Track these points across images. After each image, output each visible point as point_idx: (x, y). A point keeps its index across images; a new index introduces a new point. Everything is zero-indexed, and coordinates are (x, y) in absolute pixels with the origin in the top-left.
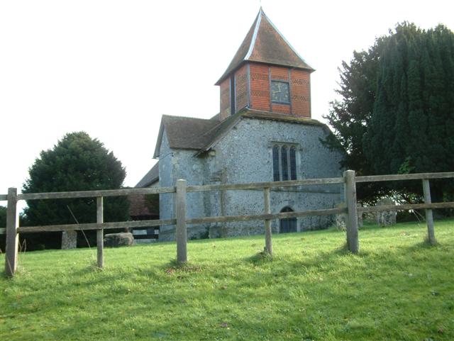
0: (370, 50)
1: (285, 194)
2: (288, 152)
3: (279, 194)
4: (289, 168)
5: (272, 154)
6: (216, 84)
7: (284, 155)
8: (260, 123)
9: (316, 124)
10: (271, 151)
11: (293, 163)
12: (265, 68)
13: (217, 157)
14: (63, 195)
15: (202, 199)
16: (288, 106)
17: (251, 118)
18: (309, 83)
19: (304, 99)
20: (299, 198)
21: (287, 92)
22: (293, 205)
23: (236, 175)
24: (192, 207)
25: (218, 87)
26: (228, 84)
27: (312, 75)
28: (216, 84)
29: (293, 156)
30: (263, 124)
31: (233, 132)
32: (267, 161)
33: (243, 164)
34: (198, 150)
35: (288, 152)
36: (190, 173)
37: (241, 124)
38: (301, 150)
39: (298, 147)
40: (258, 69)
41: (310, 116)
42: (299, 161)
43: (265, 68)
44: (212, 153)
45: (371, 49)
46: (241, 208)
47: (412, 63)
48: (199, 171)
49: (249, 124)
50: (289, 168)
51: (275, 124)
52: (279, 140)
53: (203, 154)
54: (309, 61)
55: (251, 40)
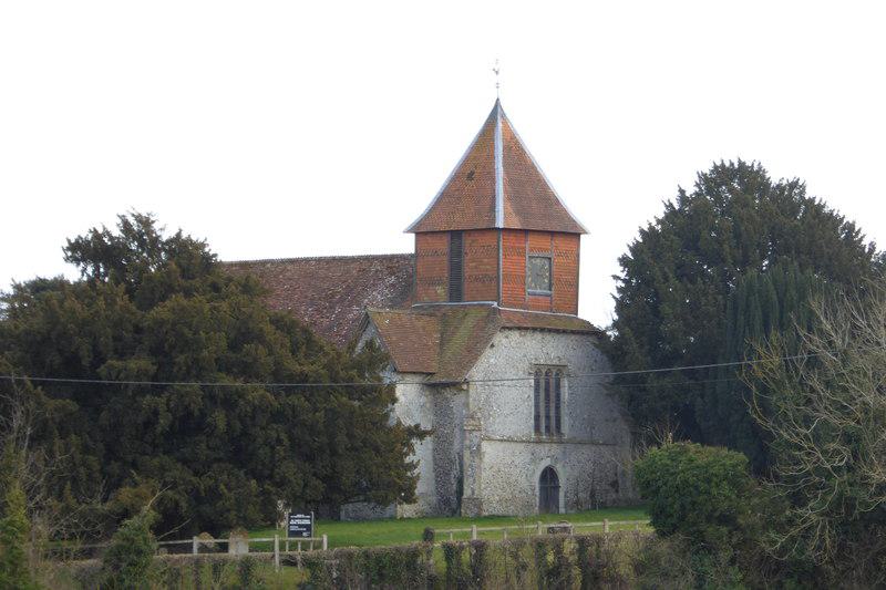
0: (832, 212)
1: (547, 447)
2: (552, 382)
3: (540, 447)
4: (553, 405)
6: (409, 231)
7: (547, 383)
8: (521, 335)
9: (588, 331)
11: (558, 396)
14: (180, 542)
15: (430, 451)
19: (567, 286)
29: (558, 386)
31: (488, 351)
41: (577, 314)
42: (565, 393)
44: (465, 387)
45: (654, 223)
46: (496, 469)
47: (132, 220)
48: (428, 405)
49: (507, 337)
50: (553, 405)
51: (538, 336)
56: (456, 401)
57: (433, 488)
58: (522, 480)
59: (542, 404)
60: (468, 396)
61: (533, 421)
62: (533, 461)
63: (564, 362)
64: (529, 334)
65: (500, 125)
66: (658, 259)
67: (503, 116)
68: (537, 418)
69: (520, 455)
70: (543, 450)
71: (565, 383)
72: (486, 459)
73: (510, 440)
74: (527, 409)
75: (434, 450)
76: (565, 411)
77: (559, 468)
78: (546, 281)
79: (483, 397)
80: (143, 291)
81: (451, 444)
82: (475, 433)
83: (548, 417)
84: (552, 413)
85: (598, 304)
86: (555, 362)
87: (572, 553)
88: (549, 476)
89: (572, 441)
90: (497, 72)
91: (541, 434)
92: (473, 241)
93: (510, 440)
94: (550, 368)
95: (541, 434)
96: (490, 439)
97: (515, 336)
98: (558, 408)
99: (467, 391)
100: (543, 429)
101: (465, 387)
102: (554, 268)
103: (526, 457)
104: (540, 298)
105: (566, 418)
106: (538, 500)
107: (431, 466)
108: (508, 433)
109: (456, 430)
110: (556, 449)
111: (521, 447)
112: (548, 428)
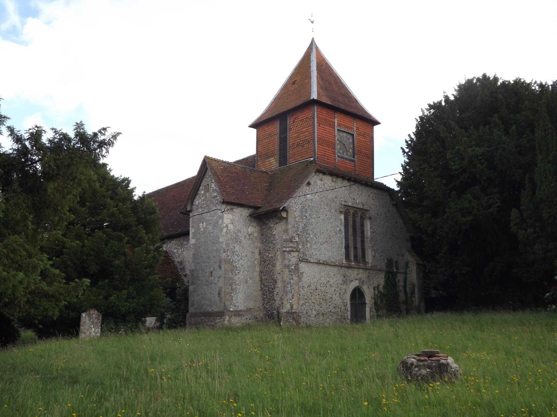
1: (356, 271)
3: (350, 271)
4: (359, 240)
5: (343, 220)
6: (252, 126)
7: (354, 222)
8: (333, 181)
10: (342, 217)
11: (363, 232)
12: (314, 112)
13: (290, 219)
15: (258, 273)
16: (353, 163)
17: (324, 173)
18: (372, 138)
20: (369, 276)
21: (352, 146)
22: (363, 284)
23: (309, 245)
24: (246, 282)
25: (254, 131)
26: (275, 128)
27: (376, 128)
28: (252, 126)
29: (362, 225)
30: (335, 182)
31: (304, 189)
32: (338, 229)
33: (315, 231)
34: (256, 208)
35: (358, 219)
36: (245, 238)
37: (314, 180)
38: (370, 218)
39: (367, 215)
40: (325, 113)
42: (368, 232)
43: (314, 112)
44: (284, 215)
46: (313, 287)
48: (255, 235)
51: (346, 183)
52: (350, 204)
53: (125, 218)
54: (371, 108)
55: (308, 77)
56: (278, 230)
57: (260, 304)
58: (336, 297)
59: (351, 238)
60: (287, 223)
61: (343, 250)
62: (344, 282)
63: (366, 207)
64: (339, 180)
65: (314, 48)
66: (436, 133)
67: (317, 48)
68: (347, 248)
69: (333, 277)
70: (353, 274)
71: (368, 225)
72: (305, 279)
73: (325, 264)
74: (339, 240)
75: (261, 272)
76: (368, 245)
77: (365, 288)
78: (351, 151)
79: (301, 225)
80: (65, 170)
81: (274, 266)
82: (292, 253)
83: (355, 248)
84: (359, 246)
85: (389, 168)
86: (360, 206)
87: (193, 244)
88: (357, 294)
89: (373, 269)
90: (312, 22)
91: (351, 261)
92: (295, 119)
93: (325, 264)
94: (356, 209)
95: (351, 261)
96: (307, 262)
97: (328, 180)
98: (363, 242)
99: (286, 219)
100: (352, 258)
101: (284, 215)
102: (356, 142)
103: (339, 279)
104: (346, 161)
105: (370, 250)
106: (349, 313)
107: (258, 286)
108: (323, 258)
109: (278, 253)
110: (362, 274)
111: (334, 270)
112: (356, 256)
